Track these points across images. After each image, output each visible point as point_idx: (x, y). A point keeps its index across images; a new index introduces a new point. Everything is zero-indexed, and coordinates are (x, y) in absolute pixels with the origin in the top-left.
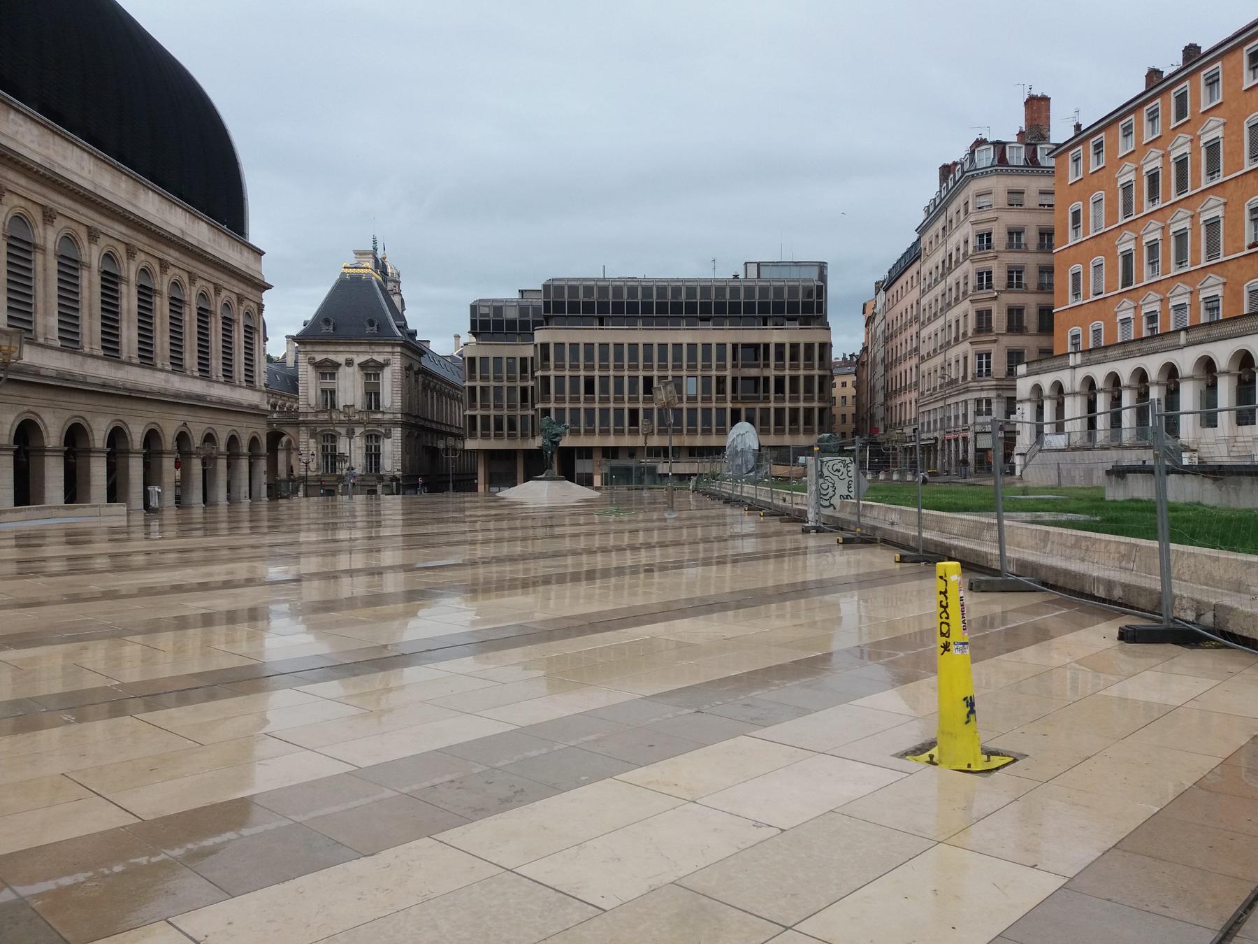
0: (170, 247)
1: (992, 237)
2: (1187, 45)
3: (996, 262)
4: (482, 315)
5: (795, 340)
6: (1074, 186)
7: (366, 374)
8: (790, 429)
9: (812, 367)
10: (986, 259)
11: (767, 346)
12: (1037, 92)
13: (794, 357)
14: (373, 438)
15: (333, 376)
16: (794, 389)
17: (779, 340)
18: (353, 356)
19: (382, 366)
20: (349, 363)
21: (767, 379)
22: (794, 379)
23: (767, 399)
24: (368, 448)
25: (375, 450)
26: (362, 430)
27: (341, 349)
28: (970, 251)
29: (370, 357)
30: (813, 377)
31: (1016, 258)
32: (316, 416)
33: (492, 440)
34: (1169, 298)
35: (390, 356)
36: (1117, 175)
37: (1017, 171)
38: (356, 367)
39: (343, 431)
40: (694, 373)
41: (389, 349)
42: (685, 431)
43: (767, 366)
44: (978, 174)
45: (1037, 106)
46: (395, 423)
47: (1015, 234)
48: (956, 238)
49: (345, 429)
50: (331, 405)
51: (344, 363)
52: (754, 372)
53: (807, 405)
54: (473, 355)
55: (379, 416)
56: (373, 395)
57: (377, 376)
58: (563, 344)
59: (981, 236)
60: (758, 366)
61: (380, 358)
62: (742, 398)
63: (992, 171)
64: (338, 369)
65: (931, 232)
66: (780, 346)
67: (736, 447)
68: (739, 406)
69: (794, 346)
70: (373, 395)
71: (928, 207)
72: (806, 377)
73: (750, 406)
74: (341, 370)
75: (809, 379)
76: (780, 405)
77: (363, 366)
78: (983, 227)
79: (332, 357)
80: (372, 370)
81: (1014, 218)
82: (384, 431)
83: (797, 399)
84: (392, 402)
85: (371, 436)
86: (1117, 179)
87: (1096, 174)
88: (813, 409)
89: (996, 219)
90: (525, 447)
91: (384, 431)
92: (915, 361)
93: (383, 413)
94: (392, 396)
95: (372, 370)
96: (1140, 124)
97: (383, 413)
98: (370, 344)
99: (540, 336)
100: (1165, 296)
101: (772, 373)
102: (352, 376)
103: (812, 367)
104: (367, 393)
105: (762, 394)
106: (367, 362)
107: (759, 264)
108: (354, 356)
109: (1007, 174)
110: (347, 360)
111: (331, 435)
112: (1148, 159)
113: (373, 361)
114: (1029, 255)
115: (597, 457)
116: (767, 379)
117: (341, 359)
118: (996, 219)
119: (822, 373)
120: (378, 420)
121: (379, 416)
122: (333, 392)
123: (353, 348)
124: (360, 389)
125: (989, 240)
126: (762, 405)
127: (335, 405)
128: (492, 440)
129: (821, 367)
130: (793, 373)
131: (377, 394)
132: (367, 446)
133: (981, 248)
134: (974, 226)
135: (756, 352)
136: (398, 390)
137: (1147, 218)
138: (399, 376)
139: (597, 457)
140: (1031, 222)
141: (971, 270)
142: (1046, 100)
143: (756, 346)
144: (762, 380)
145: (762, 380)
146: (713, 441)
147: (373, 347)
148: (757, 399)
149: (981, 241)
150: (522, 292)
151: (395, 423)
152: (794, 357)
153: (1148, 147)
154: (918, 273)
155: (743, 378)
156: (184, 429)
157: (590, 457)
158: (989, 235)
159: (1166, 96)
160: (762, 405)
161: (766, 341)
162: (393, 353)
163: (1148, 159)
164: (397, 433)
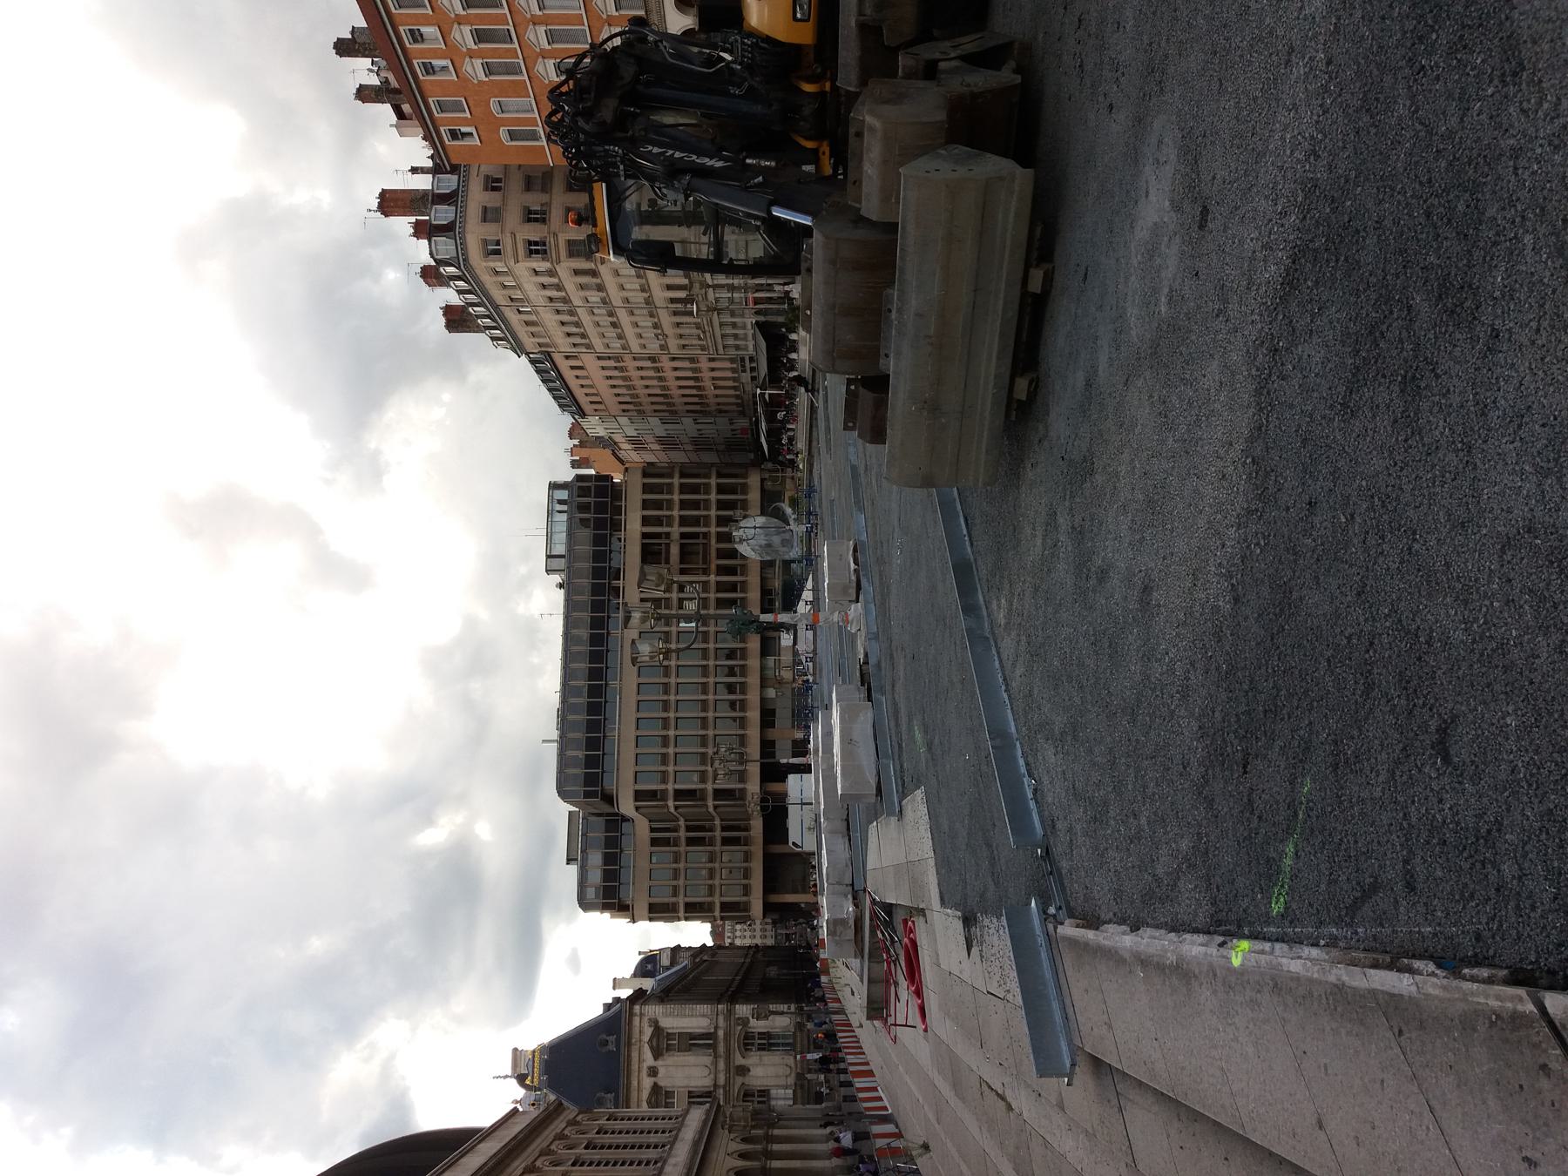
0: (509, 1165)
1: (532, 239)
2: (334, 51)
3: (560, 235)
4: (597, 897)
5: (639, 504)
6: (482, 138)
7: (667, 1050)
8: (741, 494)
9: (670, 485)
10: (557, 246)
11: (645, 536)
12: (375, 203)
13: (658, 505)
14: (750, 1042)
15: (669, 1094)
16: (695, 505)
17: (639, 521)
18: (645, 1067)
19: (658, 1030)
20: (653, 1072)
21: (683, 536)
22: (684, 505)
23: (706, 535)
24: (761, 1048)
25: (764, 1039)
26: (738, 1053)
27: (635, 1083)
28: (546, 265)
29: (646, 1045)
30: (681, 501)
31: (556, 215)
32: (719, 1087)
33: (747, 662)
34: (608, 16)
35: (646, 1019)
36: (476, 82)
37: (462, 213)
38: (660, 1063)
39: (739, 1080)
40: (672, 757)
41: (636, 1020)
42: (742, 697)
43: (668, 535)
44: (463, 254)
45: (391, 203)
46: (730, 1012)
47: (530, 217)
48: (531, 287)
49: (737, 1078)
50: (706, 1097)
51: (653, 1079)
52: (675, 550)
53: (714, 506)
54: (647, 907)
55: (721, 1033)
56: (690, 1042)
57: (670, 1036)
58: (644, 484)
59: (531, 252)
60: (668, 545)
61: (648, 1031)
62: (704, 563)
63: (460, 238)
64: (662, 1029)
65: (522, 333)
66: (646, 521)
67: (761, 546)
68: (713, 567)
69: (646, 505)
70: (690, 1042)
71: (493, 339)
72: (681, 492)
73: (713, 554)
74: (661, 1084)
75: (684, 489)
76: (714, 521)
77: (657, 1054)
78: (521, 251)
79: (645, 1094)
80: (663, 1043)
81: (513, 217)
82: (740, 1028)
83: (707, 517)
84: (703, 1016)
85: (745, 1044)
86: (479, 81)
87: (472, 109)
88: (718, 485)
89: (513, 235)
90: (761, 840)
91: (740, 1028)
92: (666, 364)
93: (716, 1028)
94: (696, 1016)
95: (663, 1043)
96: (423, 53)
97: (716, 1028)
98: (629, 1044)
99: (627, 806)
100: (606, 21)
101: (676, 530)
102: (671, 1068)
103: (670, 485)
104: (690, 1050)
105: (701, 541)
106: (651, 1048)
107: (549, 557)
108: (645, 1065)
109: (464, 222)
110: (649, 1075)
111: (745, 1038)
112: (462, 42)
113: (651, 1040)
114: (554, 202)
115: (772, 734)
116: (683, 536)
117: (647, 1083)
118: (513, 235)
119: (677, 475)
120: (725, 1034)
121: (721, 1033)
122: (691, 1095)
123: (635, 1067)
124: (686, 1058)
125: (536, 243)
126: (713, 541)
127: (707, 1092)
128: (747, 662)
129: (671, 476)
130: (677, 506)
131: (693, 1036)
132: (759, 1049)
133: (545, 252)
134: (520, 259)
135: (651, 553)
136: (688, 1008)
137: (522, 44)
138: (670, 1007)
139: (772, 734)
140: (516, 200)
141: (567, 264)
142: (384, 195)
143: (644, 547)
144: (683, 541)
145: (683, 541)
146: (754, 579)
147: (634, 1041)
148: (706, 546)
149: (537, 252)
150: (569, 861)
151: (730, 1012)
152: (658, 505)
153: (449, 43)
154: (567, 357)
155: (681, 563)
156: (735, 1155)
157: (773, 743)
158: (530, 243)
159: (398, 20)
160: (713, 541)
161: (638, 536)
162: (641, 1015)
163: (462, 42)
164: (743, 1010)
